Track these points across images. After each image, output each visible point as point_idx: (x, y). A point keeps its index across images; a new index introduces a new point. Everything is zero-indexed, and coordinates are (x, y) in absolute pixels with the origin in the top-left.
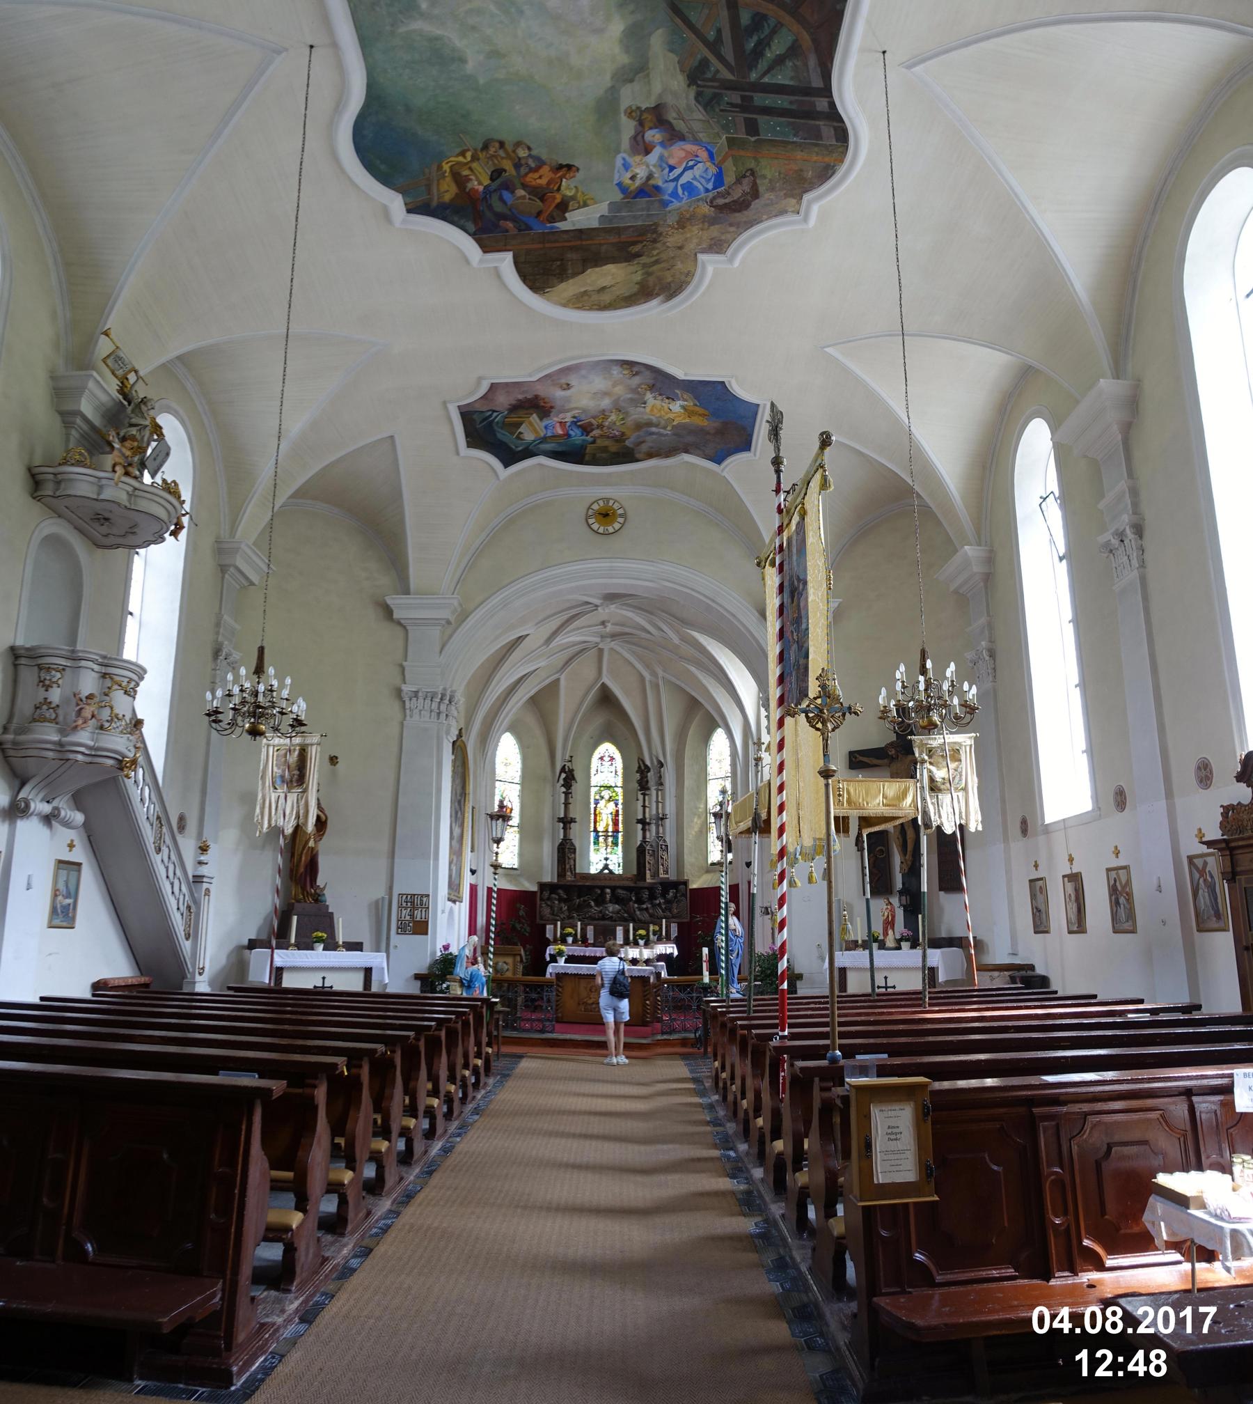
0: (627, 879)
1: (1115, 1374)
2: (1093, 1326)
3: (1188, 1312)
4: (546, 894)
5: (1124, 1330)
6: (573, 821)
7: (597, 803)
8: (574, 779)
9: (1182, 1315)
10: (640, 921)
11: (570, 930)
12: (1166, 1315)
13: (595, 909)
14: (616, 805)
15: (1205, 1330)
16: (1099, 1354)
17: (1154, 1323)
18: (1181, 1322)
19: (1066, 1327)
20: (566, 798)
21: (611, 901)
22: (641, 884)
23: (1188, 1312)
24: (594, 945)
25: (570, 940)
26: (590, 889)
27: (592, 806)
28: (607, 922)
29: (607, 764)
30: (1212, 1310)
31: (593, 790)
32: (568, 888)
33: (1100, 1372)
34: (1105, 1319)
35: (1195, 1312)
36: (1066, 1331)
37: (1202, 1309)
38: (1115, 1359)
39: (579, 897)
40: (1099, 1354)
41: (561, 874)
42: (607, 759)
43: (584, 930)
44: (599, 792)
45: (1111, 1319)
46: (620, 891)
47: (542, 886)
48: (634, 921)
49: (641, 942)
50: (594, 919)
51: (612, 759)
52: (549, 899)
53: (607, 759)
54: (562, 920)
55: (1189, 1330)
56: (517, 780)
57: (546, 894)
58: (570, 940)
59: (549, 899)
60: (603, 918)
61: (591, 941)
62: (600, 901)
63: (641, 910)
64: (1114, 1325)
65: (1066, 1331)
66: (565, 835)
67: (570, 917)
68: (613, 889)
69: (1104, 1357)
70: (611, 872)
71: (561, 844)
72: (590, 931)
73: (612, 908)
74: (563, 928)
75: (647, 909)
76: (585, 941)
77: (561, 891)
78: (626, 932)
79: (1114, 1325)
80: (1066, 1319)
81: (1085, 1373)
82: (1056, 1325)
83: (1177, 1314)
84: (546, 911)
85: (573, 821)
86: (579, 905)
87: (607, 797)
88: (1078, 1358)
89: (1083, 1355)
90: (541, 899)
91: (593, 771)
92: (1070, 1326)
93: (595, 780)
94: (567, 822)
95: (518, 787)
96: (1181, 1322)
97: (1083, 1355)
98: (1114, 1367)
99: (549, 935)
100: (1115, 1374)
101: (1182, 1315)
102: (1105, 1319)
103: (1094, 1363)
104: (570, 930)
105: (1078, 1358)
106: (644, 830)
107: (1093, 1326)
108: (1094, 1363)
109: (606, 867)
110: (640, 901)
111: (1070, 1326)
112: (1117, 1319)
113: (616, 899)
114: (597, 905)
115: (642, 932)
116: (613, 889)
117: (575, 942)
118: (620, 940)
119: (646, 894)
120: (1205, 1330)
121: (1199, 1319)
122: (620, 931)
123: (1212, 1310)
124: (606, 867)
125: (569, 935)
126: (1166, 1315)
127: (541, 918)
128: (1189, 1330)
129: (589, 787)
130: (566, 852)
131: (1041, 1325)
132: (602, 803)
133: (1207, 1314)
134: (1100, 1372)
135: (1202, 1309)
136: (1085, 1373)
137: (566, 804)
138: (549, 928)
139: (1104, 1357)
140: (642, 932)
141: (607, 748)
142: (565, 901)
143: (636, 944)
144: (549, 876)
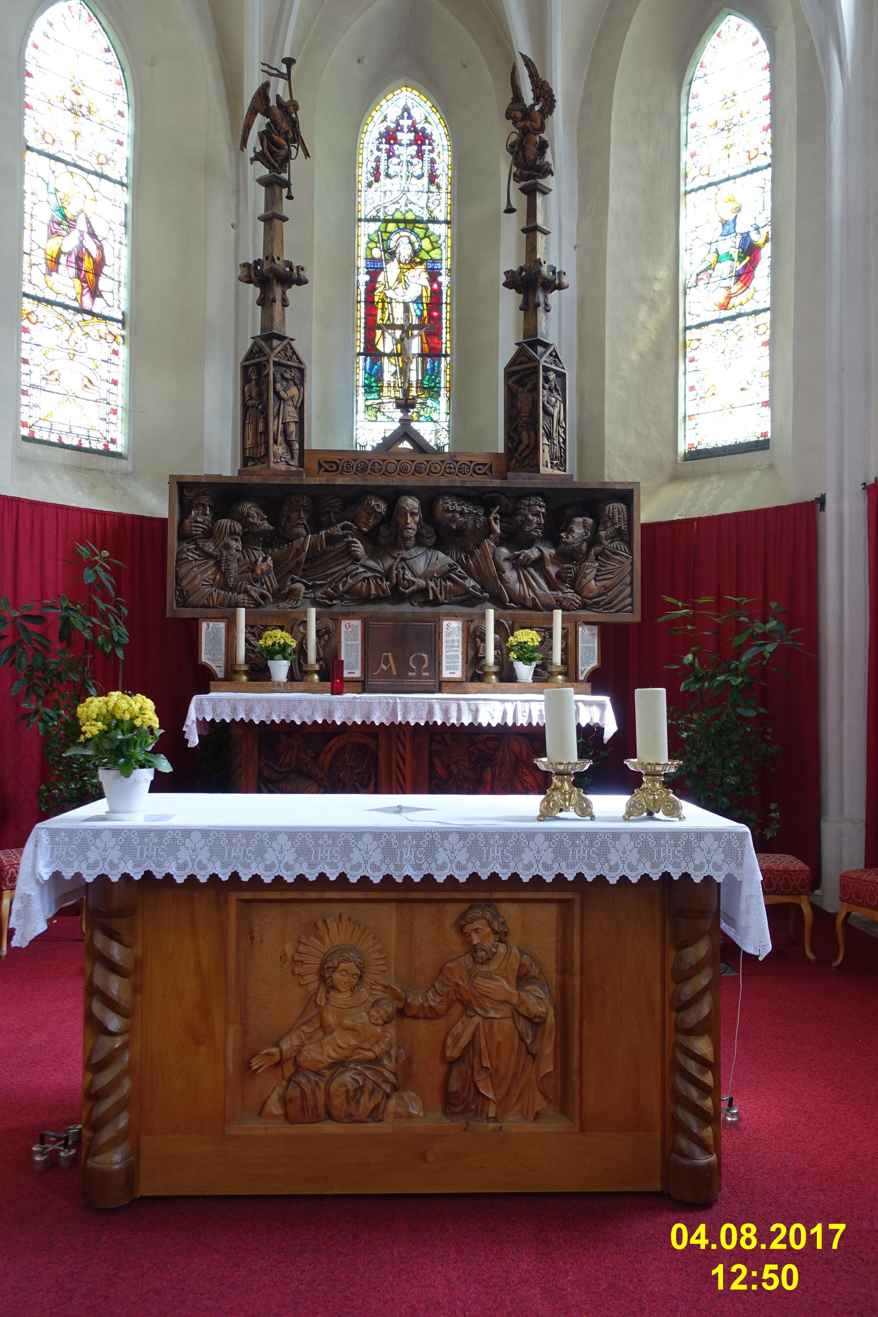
0: (476, 468)
1: (749, 1287)
2: (729, 1242)
3: (818, 1229)
4: (200, 518)
5: (758, 1246)
6: (291, 277)
7: (374, 273)
8: (297, 138)
9: (812, 1232)
10: (520, 603)
11: (280, 636)
12: (798, 1231)
13: (366, 566)
14: (433, 276)
15: (835, 1246)
16: (734, 1269)
17: (786, 1240)
18: (811, 1239)
19: (703, 1243)
20: (272, 201)
21: (420, 541)
22: (520, 480)
23: (818, 1229)
24: (363, 685)
25: (280, 669)
26: (354, 497)
27: (363, 279)
28: (406, 608)
29: (406, 152)
30: (841, 1227)
31: (367, 230)
32: (276, 499)
33: (735, 1286)
34: (740, 1235)
35: (825, 1230)
36: (703, 1247)
37: (832, 1226)
38: (749, 1274)
39: (315, 525)
40: (734, 1269)
41: (253, 452)
42: (405, 137)
43: (328, 636)
44: (383, 238)
45: (746, 1236)
46: (451, 504)
47: (187, 492)
48: (497, 601)
49: (525, 671)
50: (366, 599)
51: (421, 138)
52: (209, 534)
53: (405, 137)
54: (255, 605)
55: (819, 1246)
56: (119, 169)
57: (200, 518)
58: (280, 669)
59: (209, 534)
60: (397, 595)
61: (353, 670)
62: (386, 537)
63: (518, 565)
64: (748, 1242)
65: (703, 1247)
66: (268, 320)
67: (283, 595)
68: (430, 498)
69: (739, 1271)
70: (420, 446)
71: (251, 355)
72: (350, 637)
73: (423, 562)
74: (255, 630)
75: (539, 564)
76: (331, 675)
77: (251, 509)
78: (473, 638)
79: (748, 1242)
80: (703, 1236)
81: (721, 1287)
82: (693, 1241)
83: (808, 1232)
84: (201, 576)
85: (291, 277)
86: (314, 556)
87: (405, 252)
88: (714, 1272)
89: (719, 1270)
90: (183, 537)
91: (364, 174)
92: (707, 1242)
93: (371, 200)
94: (271, 279)
95: (124, 197)
96: (811, 1239)
97: (719, 1270)
98: (748, 1281)
99: (211, 654)
100: (749, 1287)
101: (812, 1232)
102: (740, 1235)
103: (730, 1277)
104: (280, 636)
105: (714, 1272)
106: (529, 308)
107: (729, 1242)
108: (730, 1277)
109: (405, 432)
110: (515, 538)
111: (707, 1242)
112: (751, 1236)
113: (440, 535)
114: (372, 554)
115: (529, 637)
116: (430, 498)
117: (297, 675)
118: (452, 666)
119: (535, 516)
120: (835, 1246)
121: (828, 1235)
122: (452, 632)
123: (841, 1227)
124: (405, 432)
125: (281, 651)
126: (798, 1231)
127: (184, 599)
128: (819, 1246)
129: (352, 220)
130: (268, 376)
131: (679, 1241)
132: (392, 269)
133: (837, 1230)
134: (735, 1286)
135: (832, 1226)
136: (721, 1287)
137: (272, 219)
138: (211, 633)
139: (739, 1271)
140: (529, 637)
141: (405, 104)
142: (269, 542)
143: (507, 676)
144: (218, 455)
